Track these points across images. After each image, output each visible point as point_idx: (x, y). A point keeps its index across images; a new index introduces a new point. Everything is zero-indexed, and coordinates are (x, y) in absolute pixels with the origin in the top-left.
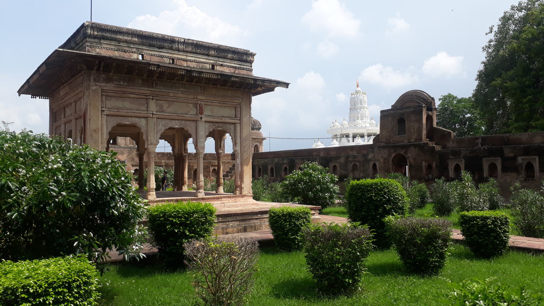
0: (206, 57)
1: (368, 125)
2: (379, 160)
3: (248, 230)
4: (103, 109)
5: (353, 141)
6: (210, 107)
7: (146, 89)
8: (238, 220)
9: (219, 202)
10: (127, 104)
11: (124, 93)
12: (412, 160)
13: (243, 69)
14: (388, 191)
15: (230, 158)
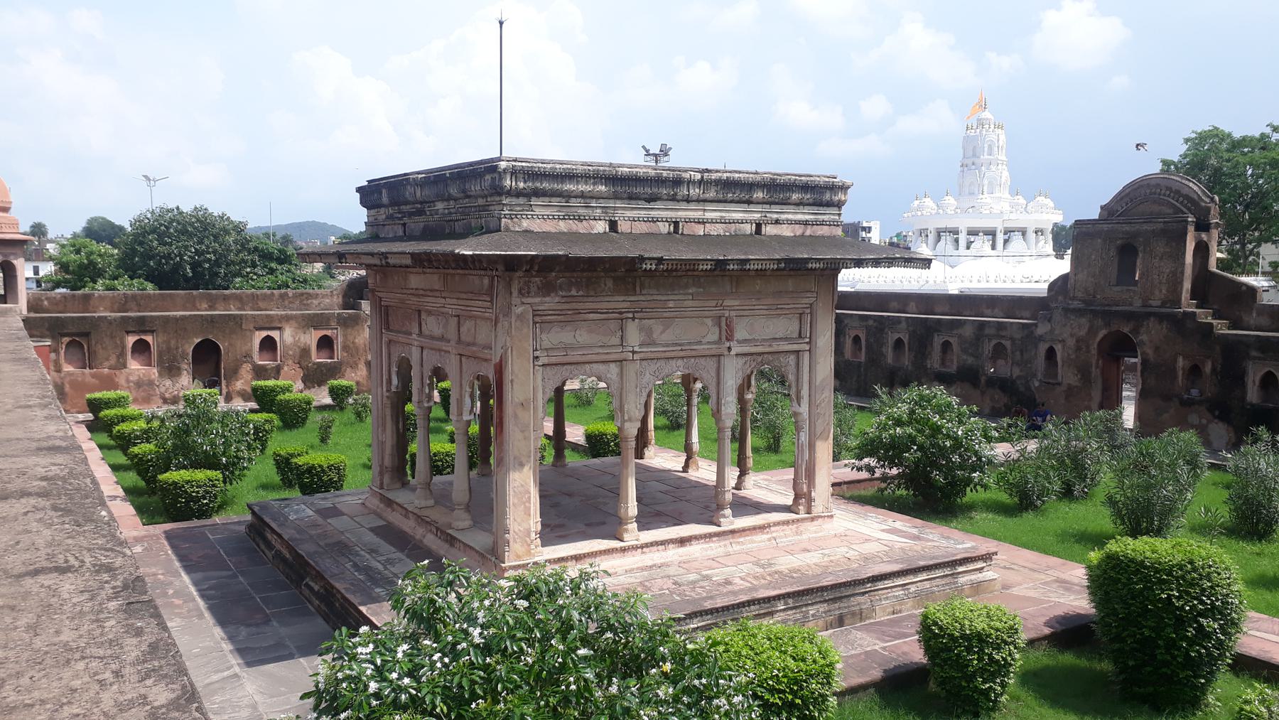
0: (744, 207)
1: (1006, 207)
2: (1063, 341)
3: (846, 622)
4: (537, 353)
5: (968, 248)
7: (622, 298)
8: (825, 601)
10: (583, 336)
12: (1150, 352)
13: (822, 223)
14: (1212, 587)
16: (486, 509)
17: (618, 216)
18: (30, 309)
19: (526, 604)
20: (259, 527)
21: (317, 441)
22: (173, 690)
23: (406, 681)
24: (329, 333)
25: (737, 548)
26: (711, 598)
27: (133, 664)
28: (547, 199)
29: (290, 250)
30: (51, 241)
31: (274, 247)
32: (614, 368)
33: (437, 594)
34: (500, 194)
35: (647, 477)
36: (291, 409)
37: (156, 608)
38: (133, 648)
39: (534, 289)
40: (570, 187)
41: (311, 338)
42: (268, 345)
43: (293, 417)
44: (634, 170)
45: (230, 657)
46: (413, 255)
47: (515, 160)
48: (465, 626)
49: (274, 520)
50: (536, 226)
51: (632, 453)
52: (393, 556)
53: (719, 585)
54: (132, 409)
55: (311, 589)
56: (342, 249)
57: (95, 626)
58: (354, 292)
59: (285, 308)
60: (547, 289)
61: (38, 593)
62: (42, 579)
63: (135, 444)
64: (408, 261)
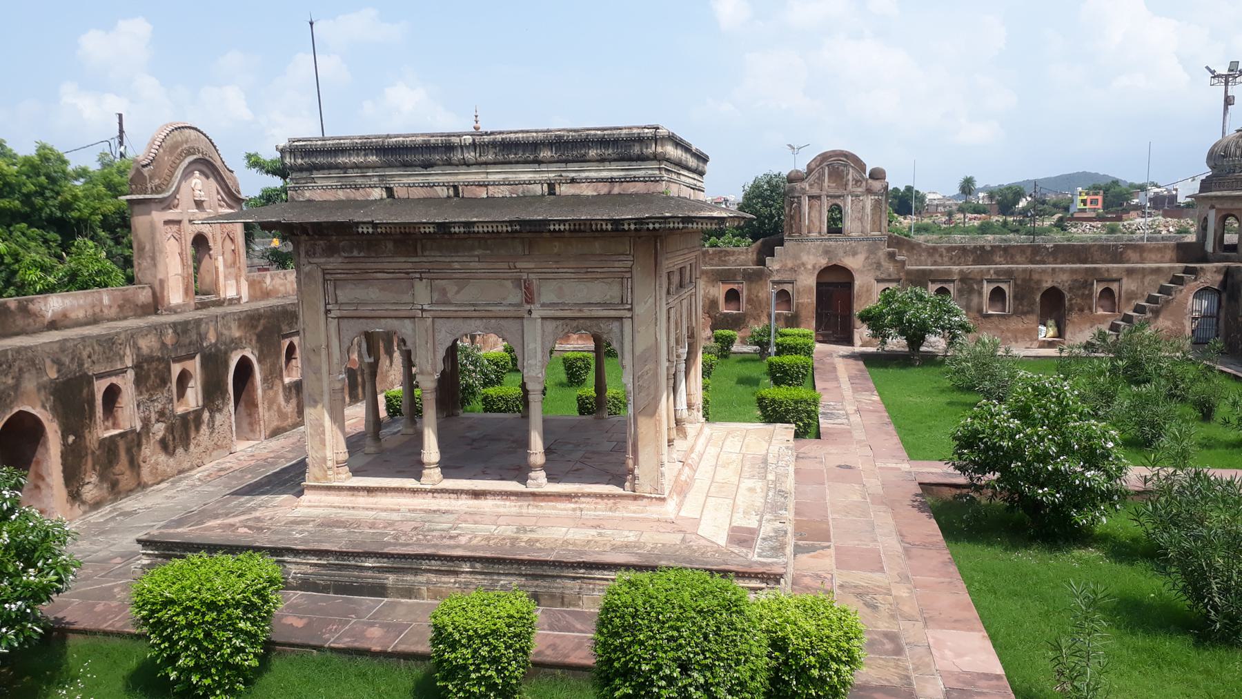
0: (536, 167)
4: (329, 307)
6: (555, 283)
7: (403, 259)
8: (520, 575)
9: (573, 506)
10: (372, 293)
13: (634, 180)
15: (1170, 254)
24: (735, 287)
25: (532, 510)
39: (319, 250)
40: (341, 160)
60: (331, 251)
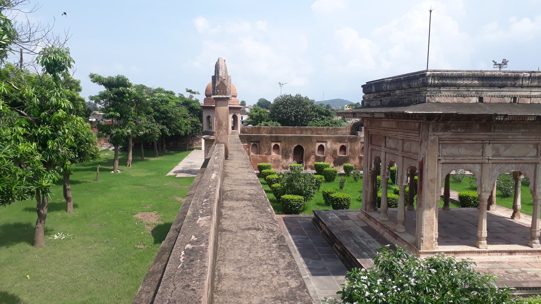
4: (440, 158)
7: (484, 134)
10: (462, 151)
11: (461, 139)
16: (413, 225)
17: (484, 95)
18: (241, 132)
19: (435, 271)
20: (317, 220)
21: (338, 188)
22: (297, 283)
23: (381, 294)
24: (344, 144)
26: (527, 282)
27: (283, 270)
28: (448, 88)
29: (329, 110)
30: (247, 107)
31: (323, 109)
32: (478, 168)
33: (394, 260)
34: (426, 86)
35: (492, 219)
36: (329, 174)
37: (289, 249)
38: (282, 264)
39: (440, 128)
41: (337, 146)
42: (321, 148)
43: (330, 177)
44: (493, 73)
45: (306, 270)
46: (386, 114)
47: (434, 71)
48: (407, 276)
49: (323, 218)
50: (443, 100)
51: (485, 207)
52: (370, 239)
53: (531, 276)
54: (272, 170)
55: (337, 248)
56: (355, 111)
57: (269, 252)
58: (356, 128)
59: (328, 134)
60: (446, 129)
61: (250, 237)
62: (250, 231)
63: (273, 183)
64: (383, 116)
